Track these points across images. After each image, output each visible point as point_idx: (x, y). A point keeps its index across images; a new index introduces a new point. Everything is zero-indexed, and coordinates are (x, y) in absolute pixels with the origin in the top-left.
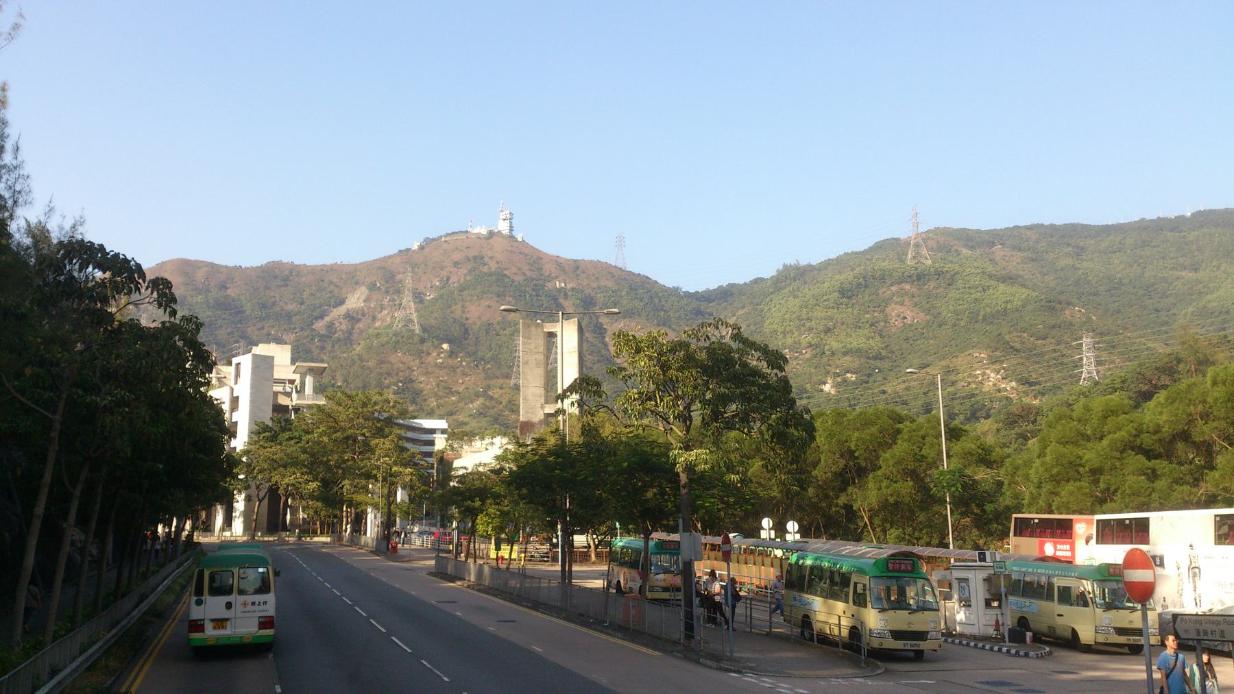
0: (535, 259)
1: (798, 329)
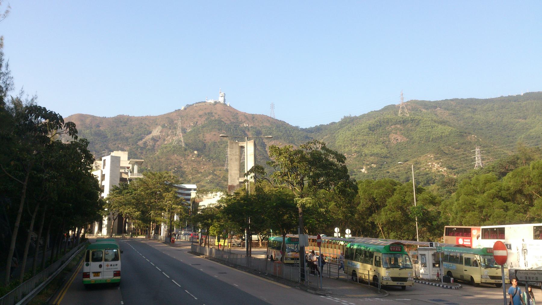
0: (235, 114)
1: (351, 144)
